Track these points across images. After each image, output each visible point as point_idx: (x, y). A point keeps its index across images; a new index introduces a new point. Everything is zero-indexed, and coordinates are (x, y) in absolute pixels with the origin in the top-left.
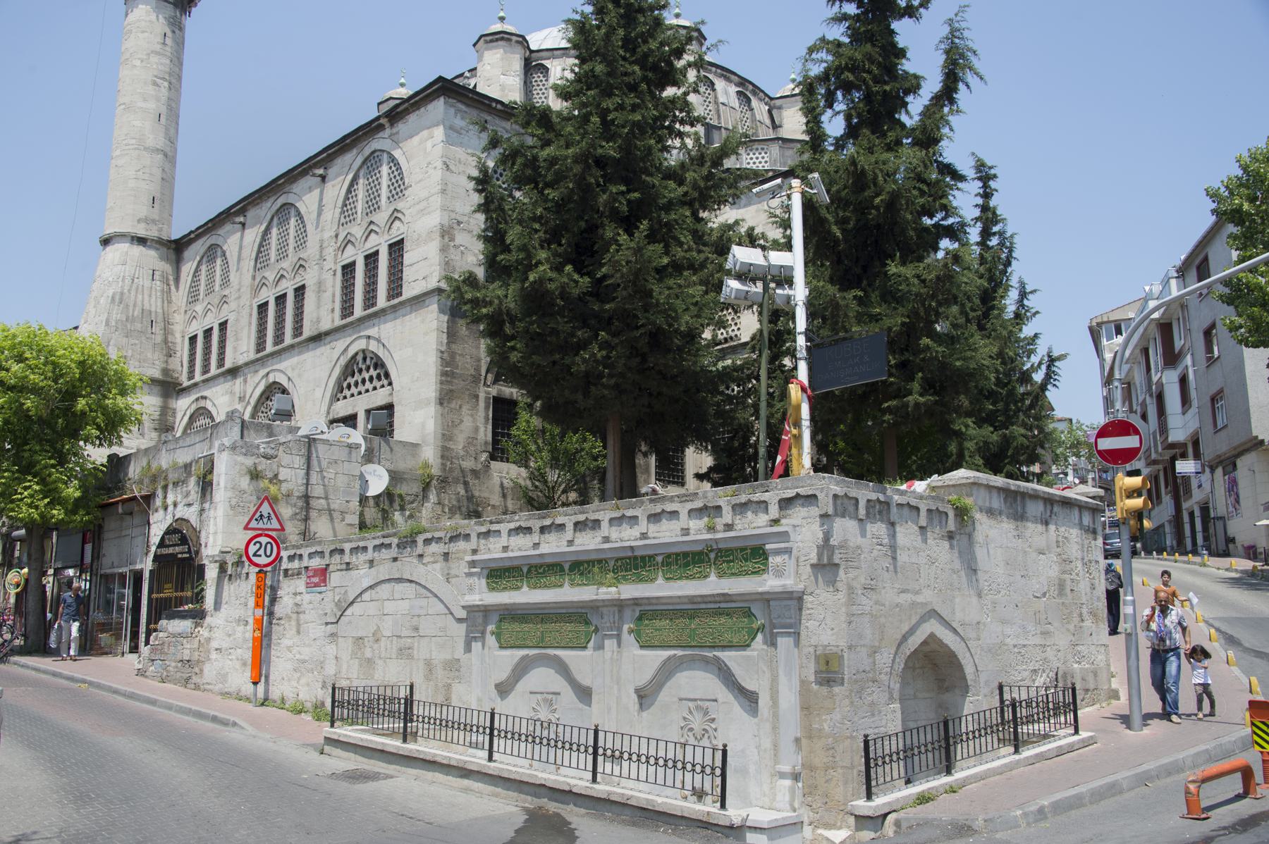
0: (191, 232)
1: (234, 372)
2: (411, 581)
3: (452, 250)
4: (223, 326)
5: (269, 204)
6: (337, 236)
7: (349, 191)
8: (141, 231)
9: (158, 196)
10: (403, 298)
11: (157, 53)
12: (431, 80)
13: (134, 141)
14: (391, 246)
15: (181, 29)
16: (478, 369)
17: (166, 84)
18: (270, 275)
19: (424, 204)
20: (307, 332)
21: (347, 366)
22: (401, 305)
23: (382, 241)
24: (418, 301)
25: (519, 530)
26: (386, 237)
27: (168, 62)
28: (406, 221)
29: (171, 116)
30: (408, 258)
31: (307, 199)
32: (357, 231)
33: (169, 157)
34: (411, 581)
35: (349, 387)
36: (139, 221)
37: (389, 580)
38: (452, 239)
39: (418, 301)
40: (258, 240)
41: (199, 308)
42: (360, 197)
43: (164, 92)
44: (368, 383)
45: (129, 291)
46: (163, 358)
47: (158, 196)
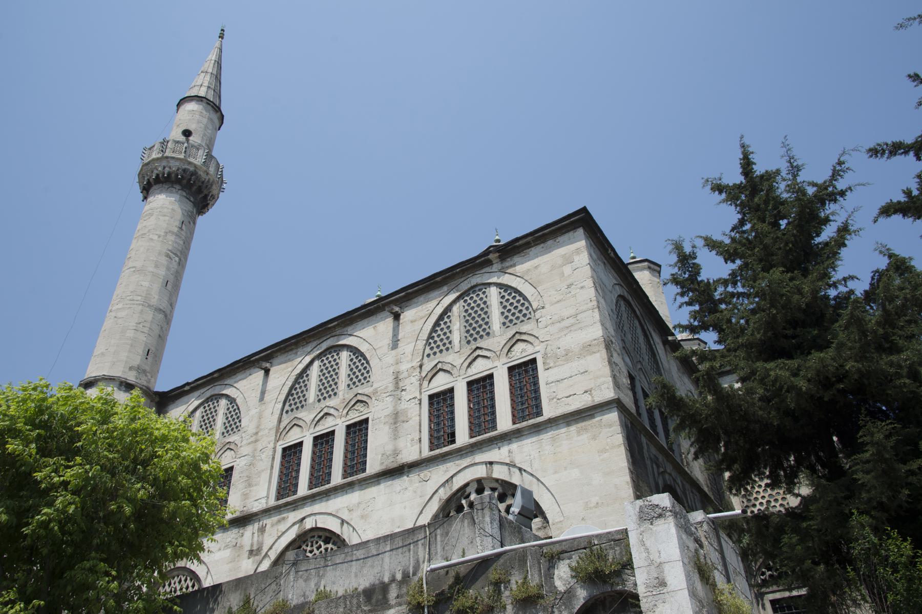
0: (188, 384)
1: (242, 521)
5: (309, 349)
6: (421, 366)
8: (131, 377)
9: (153, 349)
11: (173, 233)
12: (519, 235)
13: (139, 298)
14: (316, 439)
15: (194, 223)
17: (177, 259)
21: (449, 501)
26: (312, 431)
27: (181, 242)
29: (172, 285)
31: (245, 388)
33: (166, 316)
36: (131, 368)
40: (289, 384)
43: (174, 265)
47: (153, 349)
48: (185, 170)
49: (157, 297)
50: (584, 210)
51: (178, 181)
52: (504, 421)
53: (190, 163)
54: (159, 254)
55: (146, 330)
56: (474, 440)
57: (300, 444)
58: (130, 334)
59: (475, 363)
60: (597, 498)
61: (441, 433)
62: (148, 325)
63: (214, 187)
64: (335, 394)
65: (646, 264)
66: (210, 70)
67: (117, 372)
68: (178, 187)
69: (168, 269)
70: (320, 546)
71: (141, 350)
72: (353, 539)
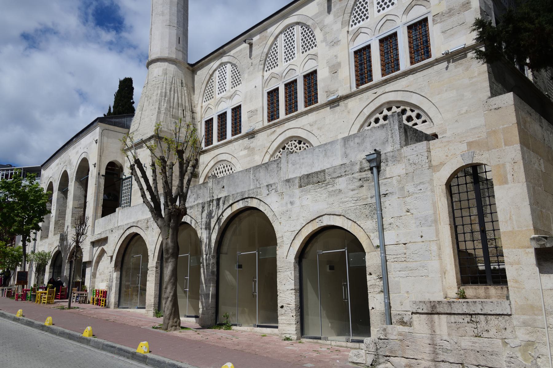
52: (405, 63)
56: (385, 78)
57: (277, 89)
60: (467, 107)
61: (363, 73)
64: (316, 46)
70: (296, 146)
72: (315, 142)
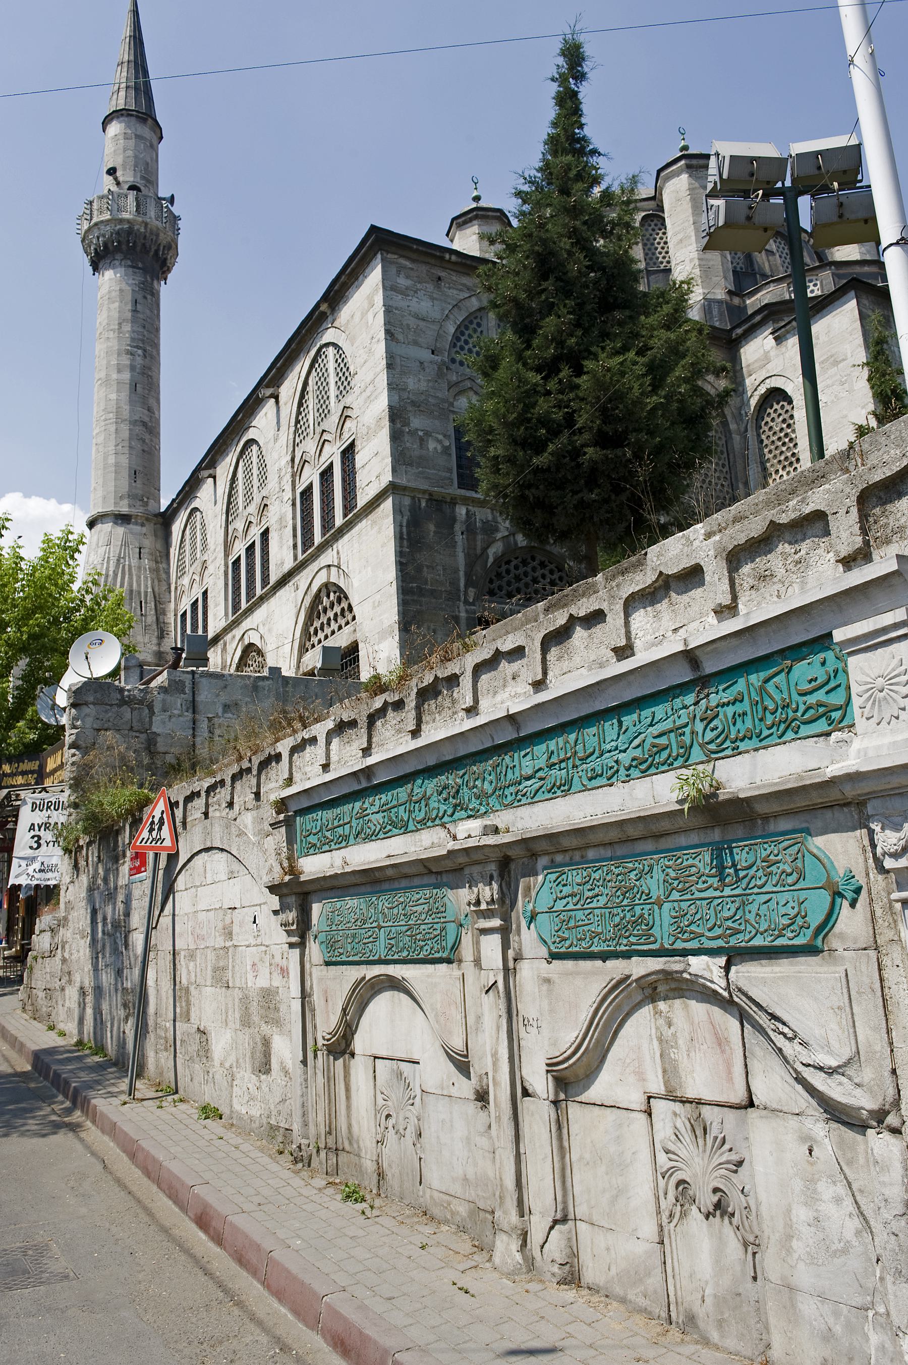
0: (174, 501)
2: (222, 850)
3: (407, 438)
4: (205, 593)
6: (293, 460)
7: (300, 404)
8: (125, 509)
10: (359, 506)
16: (454, 583)
18: (239, 525)
19: (371, 388)
20: (273, 579)
22: (356, 515)
23: (335, 449)
24: (374, 504)
25: (342, 727)
28: (354, 416)
30: (360, 460)
32: (309, 446)
34: (222, 850)
35: (316, 633)
37: (200, 852)
38: (406, 423)
39: (374, 504)
41: (186, 581)
42: (311, 407)
43: (139, 360)
44: (333, 622)
45: (115, 575)
46: (155, 641)
48: (118, 233)
49: (127, 407)
50: (373, 229)
51: (118, 249)
53: (121, 221)
54: (119, 355)
55: (126, 450)
58: (112, 460)
59: (324, 450)
62: (126, 444)
63: (162, 235)
65: (683, 162)
66: (126, 58)
67: (110, 508)
68: (119, 256)
69: (132, 368)
71: (125, 474)
